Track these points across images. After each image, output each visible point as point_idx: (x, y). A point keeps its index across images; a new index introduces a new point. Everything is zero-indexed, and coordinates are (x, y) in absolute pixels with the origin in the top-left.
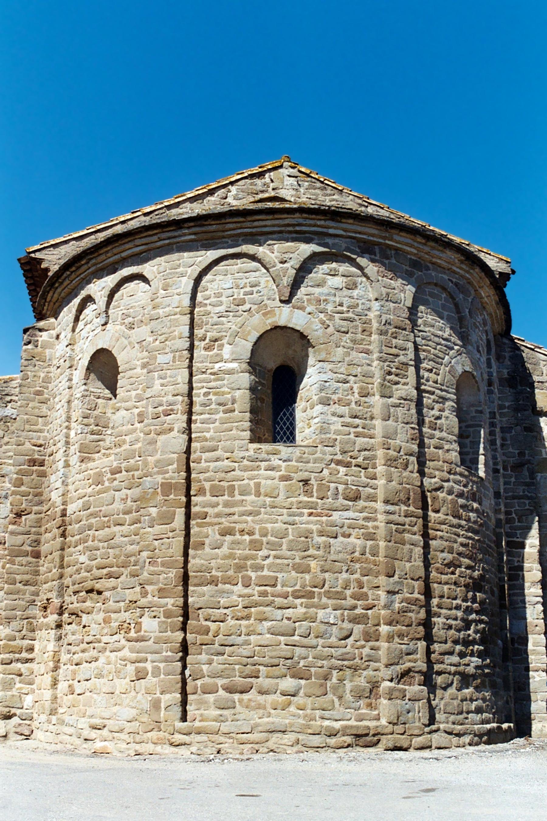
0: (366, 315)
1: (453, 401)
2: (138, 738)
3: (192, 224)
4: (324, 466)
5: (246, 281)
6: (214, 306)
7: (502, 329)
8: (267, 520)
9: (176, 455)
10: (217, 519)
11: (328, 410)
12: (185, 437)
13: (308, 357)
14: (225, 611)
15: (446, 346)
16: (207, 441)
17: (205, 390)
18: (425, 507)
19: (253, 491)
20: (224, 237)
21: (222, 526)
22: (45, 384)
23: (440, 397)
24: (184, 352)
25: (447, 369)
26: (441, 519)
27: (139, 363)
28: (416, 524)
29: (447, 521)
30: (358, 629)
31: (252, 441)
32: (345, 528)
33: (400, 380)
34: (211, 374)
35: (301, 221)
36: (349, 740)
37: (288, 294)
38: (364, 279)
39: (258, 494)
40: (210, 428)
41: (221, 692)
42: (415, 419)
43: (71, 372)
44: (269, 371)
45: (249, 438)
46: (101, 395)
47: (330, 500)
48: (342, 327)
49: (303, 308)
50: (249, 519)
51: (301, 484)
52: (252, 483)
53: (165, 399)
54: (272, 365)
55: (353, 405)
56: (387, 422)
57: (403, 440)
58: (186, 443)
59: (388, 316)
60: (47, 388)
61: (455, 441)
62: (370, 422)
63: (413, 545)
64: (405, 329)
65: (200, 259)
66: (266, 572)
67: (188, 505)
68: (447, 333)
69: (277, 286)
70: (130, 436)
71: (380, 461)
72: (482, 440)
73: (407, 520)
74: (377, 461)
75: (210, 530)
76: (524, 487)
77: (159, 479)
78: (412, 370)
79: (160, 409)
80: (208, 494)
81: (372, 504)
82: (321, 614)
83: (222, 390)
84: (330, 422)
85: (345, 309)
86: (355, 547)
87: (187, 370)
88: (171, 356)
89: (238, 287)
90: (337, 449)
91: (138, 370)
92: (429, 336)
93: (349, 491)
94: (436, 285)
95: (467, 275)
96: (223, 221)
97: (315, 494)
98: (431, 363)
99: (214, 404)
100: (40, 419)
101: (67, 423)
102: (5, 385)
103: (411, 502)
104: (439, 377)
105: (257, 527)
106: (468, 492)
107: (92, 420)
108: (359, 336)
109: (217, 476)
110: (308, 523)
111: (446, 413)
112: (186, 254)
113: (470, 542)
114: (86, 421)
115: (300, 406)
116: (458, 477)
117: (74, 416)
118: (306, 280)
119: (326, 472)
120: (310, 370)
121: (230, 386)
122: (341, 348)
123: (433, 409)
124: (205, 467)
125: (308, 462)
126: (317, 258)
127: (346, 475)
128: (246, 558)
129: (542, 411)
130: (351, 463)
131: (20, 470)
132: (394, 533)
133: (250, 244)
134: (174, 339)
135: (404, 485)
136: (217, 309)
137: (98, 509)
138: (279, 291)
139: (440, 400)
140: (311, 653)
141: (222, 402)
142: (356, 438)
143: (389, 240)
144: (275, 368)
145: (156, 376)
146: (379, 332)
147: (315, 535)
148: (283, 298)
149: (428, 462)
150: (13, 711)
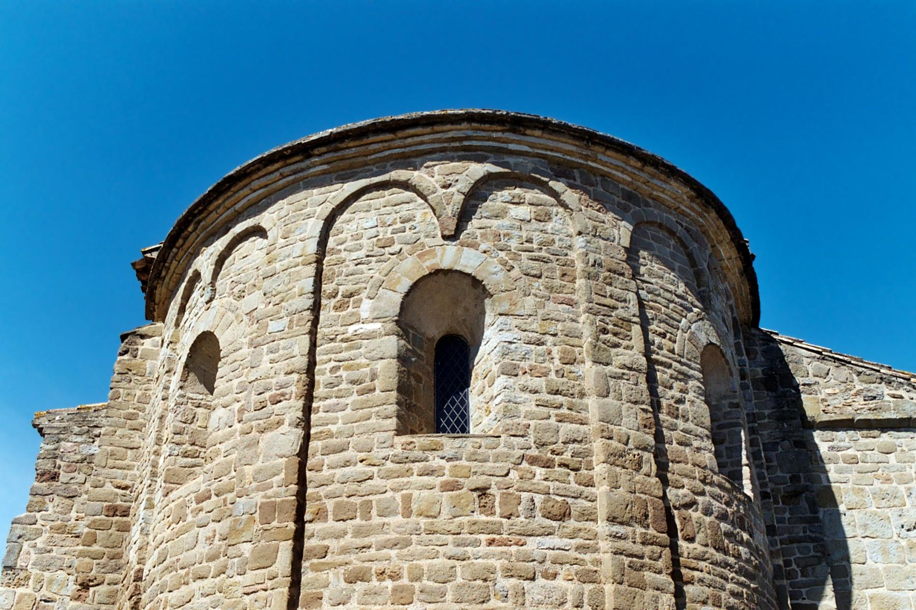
0: (566, 255)
1: (698, 379)
3: (324, 149)
4: (511, 466)
5: (395, 216)
6: (350, 251)
7: (749, 317)
8: (421, 554)
9: (285, 459)
10: (342, 556)
11: (514, 383)
12: (300, 432)
13: (485, 313)
15: (681, 305)
16: (332, 437)
17: (333, 364)
18: (672, 531)
19: (400, 509)
20: (367, 164)
21: (350, 567)
22: (140, 405)
23: (680, 372)
24: (304, 313)
25: (686, 335)
26: (698, 551)
27: (246, 340)
28: (660, 557)
29: (706, 556)
31: (399, 432)
32: (548, 564)
33: (621, 341)
34: (342, 340)
35: (470, 133)
37: (453, 227)
38: (561, 210)
39: (407, 513)
40: (337, 418)
42: (646, 396)
43: (168, 378)
44: (429, 340)
45: (394, 427)
46: (203, 402)
47: (522, 519)
48: (532, 268)
49: (475, 246)
50: (393, 553)
51: (475, 494)
52: (398, 496)
53: (274, 381)
54: (434, 331)
55: (553, 375)
56: (606, 399)
57: (631, 424)
58: (301, 441)
59: (598, 256)
60: (143, 410)
61: (707, 436)
62: (579, 401)
63: (658, 589)
64: (623, 275)
65: (334, 194)
67: (299, 537)
68: (682, 288)
69: (438, 218)
70: (227, 442)
71: (598, 456)
72: (743, 444)
73: (648, 549)
74: (594, 458)
75: (331, 575)
76: (804, 525)
77: (258, 498)
78: (636, 330)
79: (267, 395)
80: (330, 517)
81: (590, 525)
83: (358, 361)
84: (518, 400)
85: (535, 246)
86: (564, 594)
87: (307, 336)
88: (286, 320)
89: (384, 224)
90: (531, 439)
92: (656, 290)
93: (550, 504)
94: (660, 226)
95: (701, 220)
96: (365, 141)
97: (498, 510)
98: (662, 325)
99: (345, 382)
100: (129, 452)
101: (156, 447)
102: (96, 414)
103: (650, 521)
104: (676, 346)
105: (406, 566)
106: (733, 513)
108: (558, 282)
109: (346, 489)
110: (486, 556)
111: (691, 396)
112: (315, 191)
113: (745, 590)
114: (177, 438)
115: (476, 384)
116: (717, 490)
117: (167, 433)
118: (479, 210)
119: (514, 475)
120: (488, 333)
121: (368, 355)
122: (532, 296)
123: (671, 388)
124: (325, 471)
125: (485, 461)
126: (494, 183)
127: (546, 479)
129: (814, 421)
130: (553, 460)
131: (94, 522)
132: (627, 570)
133: (402, 169)
135: (637, 494)
136: (354, 255)
137: (175, 559)
138: (441, 224)
139: (680, 377)
141: (356, 378)
142: (560, 424)
143: (593, 161)
144: (438, 337)
145: (265, 350)
146: (586, 274)
147: (499, 574)
148: (447, 233)
149: (670, 464)
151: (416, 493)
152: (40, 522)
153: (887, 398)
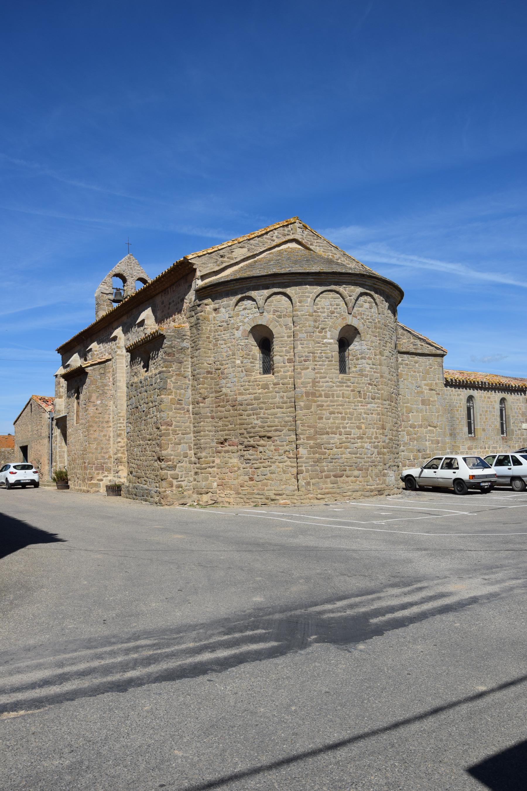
2: (302, 497)
9: (311, 380)
14: (333, 445)
17: (320, 351)
30: (376, 450)
36: (377, 493)
39: (343, 397)
41: (332, 478)
49: (356, 317)
50: (341, 407)
52: (341, 392)
65: (316, 290)
66: (348, 429)
77: (304, 390)
79: (302, 358)
80: (323, 396)
82: (366, 445)
89: (331, 305)
91: (286, 338)
107: (251, 357)
128: (340, 424)
131: (204, 376)
134: (306, 327)
140: (362, 461)
150: (209, 490)
151: (345, 392)
152: (172, 372)
153: (419, 346)
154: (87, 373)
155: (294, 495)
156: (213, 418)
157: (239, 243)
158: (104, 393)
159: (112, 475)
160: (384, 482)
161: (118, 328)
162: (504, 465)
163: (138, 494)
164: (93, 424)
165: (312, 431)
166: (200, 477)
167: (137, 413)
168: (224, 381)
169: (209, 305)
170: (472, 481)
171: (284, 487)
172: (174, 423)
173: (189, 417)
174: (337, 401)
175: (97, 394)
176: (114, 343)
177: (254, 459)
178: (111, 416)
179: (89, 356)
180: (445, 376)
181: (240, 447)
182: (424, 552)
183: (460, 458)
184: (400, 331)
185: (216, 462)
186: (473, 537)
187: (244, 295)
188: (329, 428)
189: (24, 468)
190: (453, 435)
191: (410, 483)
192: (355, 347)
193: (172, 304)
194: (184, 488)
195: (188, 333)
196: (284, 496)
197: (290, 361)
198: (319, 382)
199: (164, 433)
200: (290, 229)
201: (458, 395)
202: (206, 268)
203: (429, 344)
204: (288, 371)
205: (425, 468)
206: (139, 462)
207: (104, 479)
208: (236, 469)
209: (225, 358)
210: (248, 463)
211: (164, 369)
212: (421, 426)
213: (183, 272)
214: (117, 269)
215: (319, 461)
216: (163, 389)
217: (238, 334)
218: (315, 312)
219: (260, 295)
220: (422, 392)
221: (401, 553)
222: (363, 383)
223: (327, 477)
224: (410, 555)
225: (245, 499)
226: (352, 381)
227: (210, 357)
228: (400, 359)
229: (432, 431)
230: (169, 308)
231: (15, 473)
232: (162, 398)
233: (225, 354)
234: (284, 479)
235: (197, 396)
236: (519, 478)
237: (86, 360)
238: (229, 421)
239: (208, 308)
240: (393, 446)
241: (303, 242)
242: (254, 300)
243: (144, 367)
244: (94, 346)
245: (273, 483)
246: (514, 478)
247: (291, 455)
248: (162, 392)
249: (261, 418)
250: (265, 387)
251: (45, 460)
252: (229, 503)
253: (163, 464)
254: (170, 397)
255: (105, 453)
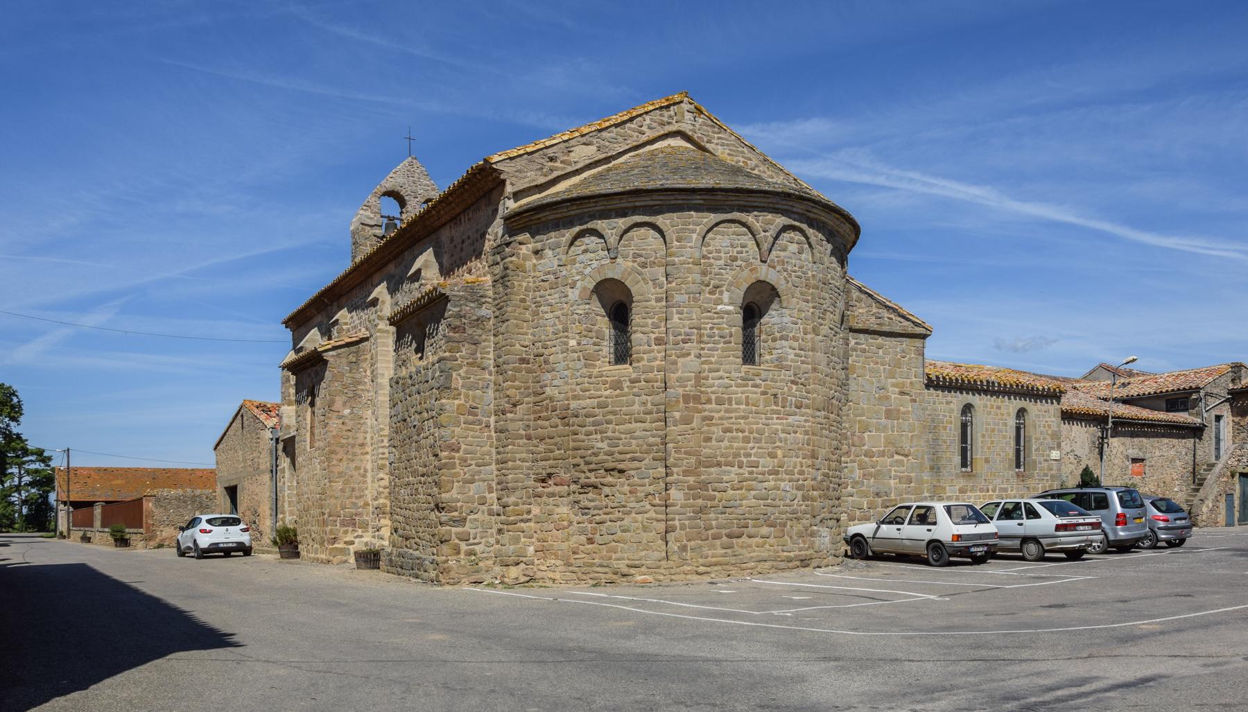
2: (672, 571)
30: (800, 493)
36: (798, 563)
39: (747, 404)
41: (725, 538)
49: (774, 267)
66: (753, 458)
77: (681, 391)
82: (782, 484)
89: (732, 246)
91: (653, 303)
140: (776, 510)
154: (326, 362)
155: (659, 567)
156: (529, 438)
157: (582, 136)
158: (356, 396)
159: (370, 534)
160: (811, 547)
161: (379, 284)
162: (1012, 518)
163: (406, 567)
164: (338, 449)
165: (693, 460)
166: (506, 537)
167: (406, 429)
168: (549, 376)
169: (526, 245)
170: (956, 544)
171: (643, 553)
172: (463, 447)
173: (490, 437)
174: (736, 410)
175: (344, 398)
176: (373, 309)
177: (596, 508)
178: (368, 436)
179: (335, 331)
180: (927, 371)
181: (573, 487)
182: (832, 663)
183: (939, 507)
184: (855, 294)
185: (533, 513)
186: (926, 637)
187: (585, 227)
188: (722, 456)
189: (226, 522)
190: (935, 469)
191: (859, 548)
192: (772, 319)
193: (467, 242)
194: (479, 555)
195: (490, 293)
196: (643, 569)
197: (659, 341)
198: (706, 378)
199: (446, 464)
200: (672, 113)
201: (948, 403)
202: (520, 175)
203: (903, 317)
204: (655, 359)
205: (883, 522)
206: (407, 513)
207: (357, 540)
208: (565, 523)
209: (551, 336)
210: (586, 514)
211: (447, 354)
212: (882, 454)
213: (482, 185)
214: (388, 183)
215: (702, 510)
216: (445, 388)
217: (573, 294)
218: (704, 257)
219: (610, 227)
220: (888, 398)
221: (795, 666)
222: (782, 381)
223: (716, 537)
224: (805, 669)
225: (580, 574)
226: (763, 377)
227: (526, 334)
228: (852, 342)
229: (898, 459)
230: (462, 250)
231: (210, 531)
232: (442, 405)
233: (551, 330)
234: (644, 541)
235: (503, 401)
236: (1035, 539)
237: (330, 339)
238: (556, 444)
239: (524, 250)
240: (832, 487)
241: (695, 137)
242: (601, 236)
243: (417, 351)
244: (343, 315)
245: (626, 547)
246: (1025, 540)
247: (657, 501)
248: (443, 394)
249: (608, 438)
250: (617, 385)
251: (265, 509)
252: (554, 580)
253: (444, 516)
254: (457, 402)
255: (357, 498)
